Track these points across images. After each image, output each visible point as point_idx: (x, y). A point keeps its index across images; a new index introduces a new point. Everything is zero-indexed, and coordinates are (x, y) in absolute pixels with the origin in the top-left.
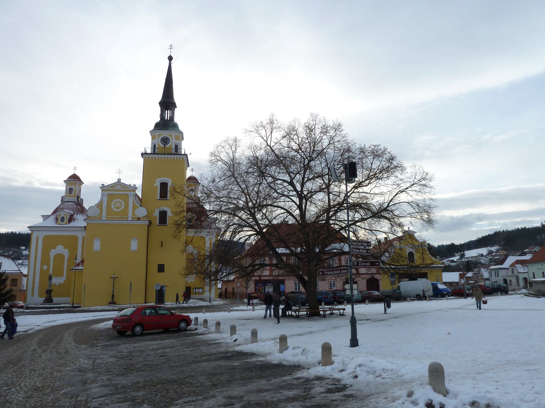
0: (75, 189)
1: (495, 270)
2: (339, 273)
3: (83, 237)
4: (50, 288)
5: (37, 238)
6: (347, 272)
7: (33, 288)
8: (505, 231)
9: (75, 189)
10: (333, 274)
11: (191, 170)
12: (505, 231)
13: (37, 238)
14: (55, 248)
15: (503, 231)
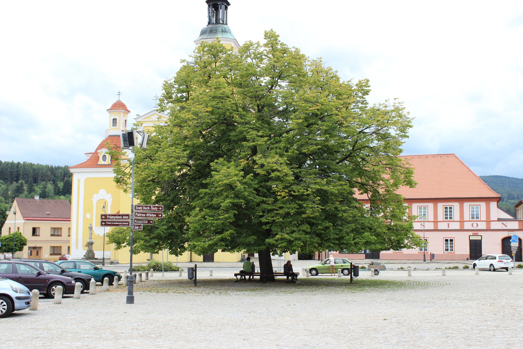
0: (120, 120)
1: (478, 228)
2: (120, 219)
3: (78, 180)
4: (91, 240)
5: (79, 181)
6: (128, 218)
7: (77, 240)
8: (54, 167)
9: (120, 120)
10: (115, 219)
11: (118, 94)
12: (54, 167)
13: (79, 181)
14: (97, 193)
15: (52, 167)
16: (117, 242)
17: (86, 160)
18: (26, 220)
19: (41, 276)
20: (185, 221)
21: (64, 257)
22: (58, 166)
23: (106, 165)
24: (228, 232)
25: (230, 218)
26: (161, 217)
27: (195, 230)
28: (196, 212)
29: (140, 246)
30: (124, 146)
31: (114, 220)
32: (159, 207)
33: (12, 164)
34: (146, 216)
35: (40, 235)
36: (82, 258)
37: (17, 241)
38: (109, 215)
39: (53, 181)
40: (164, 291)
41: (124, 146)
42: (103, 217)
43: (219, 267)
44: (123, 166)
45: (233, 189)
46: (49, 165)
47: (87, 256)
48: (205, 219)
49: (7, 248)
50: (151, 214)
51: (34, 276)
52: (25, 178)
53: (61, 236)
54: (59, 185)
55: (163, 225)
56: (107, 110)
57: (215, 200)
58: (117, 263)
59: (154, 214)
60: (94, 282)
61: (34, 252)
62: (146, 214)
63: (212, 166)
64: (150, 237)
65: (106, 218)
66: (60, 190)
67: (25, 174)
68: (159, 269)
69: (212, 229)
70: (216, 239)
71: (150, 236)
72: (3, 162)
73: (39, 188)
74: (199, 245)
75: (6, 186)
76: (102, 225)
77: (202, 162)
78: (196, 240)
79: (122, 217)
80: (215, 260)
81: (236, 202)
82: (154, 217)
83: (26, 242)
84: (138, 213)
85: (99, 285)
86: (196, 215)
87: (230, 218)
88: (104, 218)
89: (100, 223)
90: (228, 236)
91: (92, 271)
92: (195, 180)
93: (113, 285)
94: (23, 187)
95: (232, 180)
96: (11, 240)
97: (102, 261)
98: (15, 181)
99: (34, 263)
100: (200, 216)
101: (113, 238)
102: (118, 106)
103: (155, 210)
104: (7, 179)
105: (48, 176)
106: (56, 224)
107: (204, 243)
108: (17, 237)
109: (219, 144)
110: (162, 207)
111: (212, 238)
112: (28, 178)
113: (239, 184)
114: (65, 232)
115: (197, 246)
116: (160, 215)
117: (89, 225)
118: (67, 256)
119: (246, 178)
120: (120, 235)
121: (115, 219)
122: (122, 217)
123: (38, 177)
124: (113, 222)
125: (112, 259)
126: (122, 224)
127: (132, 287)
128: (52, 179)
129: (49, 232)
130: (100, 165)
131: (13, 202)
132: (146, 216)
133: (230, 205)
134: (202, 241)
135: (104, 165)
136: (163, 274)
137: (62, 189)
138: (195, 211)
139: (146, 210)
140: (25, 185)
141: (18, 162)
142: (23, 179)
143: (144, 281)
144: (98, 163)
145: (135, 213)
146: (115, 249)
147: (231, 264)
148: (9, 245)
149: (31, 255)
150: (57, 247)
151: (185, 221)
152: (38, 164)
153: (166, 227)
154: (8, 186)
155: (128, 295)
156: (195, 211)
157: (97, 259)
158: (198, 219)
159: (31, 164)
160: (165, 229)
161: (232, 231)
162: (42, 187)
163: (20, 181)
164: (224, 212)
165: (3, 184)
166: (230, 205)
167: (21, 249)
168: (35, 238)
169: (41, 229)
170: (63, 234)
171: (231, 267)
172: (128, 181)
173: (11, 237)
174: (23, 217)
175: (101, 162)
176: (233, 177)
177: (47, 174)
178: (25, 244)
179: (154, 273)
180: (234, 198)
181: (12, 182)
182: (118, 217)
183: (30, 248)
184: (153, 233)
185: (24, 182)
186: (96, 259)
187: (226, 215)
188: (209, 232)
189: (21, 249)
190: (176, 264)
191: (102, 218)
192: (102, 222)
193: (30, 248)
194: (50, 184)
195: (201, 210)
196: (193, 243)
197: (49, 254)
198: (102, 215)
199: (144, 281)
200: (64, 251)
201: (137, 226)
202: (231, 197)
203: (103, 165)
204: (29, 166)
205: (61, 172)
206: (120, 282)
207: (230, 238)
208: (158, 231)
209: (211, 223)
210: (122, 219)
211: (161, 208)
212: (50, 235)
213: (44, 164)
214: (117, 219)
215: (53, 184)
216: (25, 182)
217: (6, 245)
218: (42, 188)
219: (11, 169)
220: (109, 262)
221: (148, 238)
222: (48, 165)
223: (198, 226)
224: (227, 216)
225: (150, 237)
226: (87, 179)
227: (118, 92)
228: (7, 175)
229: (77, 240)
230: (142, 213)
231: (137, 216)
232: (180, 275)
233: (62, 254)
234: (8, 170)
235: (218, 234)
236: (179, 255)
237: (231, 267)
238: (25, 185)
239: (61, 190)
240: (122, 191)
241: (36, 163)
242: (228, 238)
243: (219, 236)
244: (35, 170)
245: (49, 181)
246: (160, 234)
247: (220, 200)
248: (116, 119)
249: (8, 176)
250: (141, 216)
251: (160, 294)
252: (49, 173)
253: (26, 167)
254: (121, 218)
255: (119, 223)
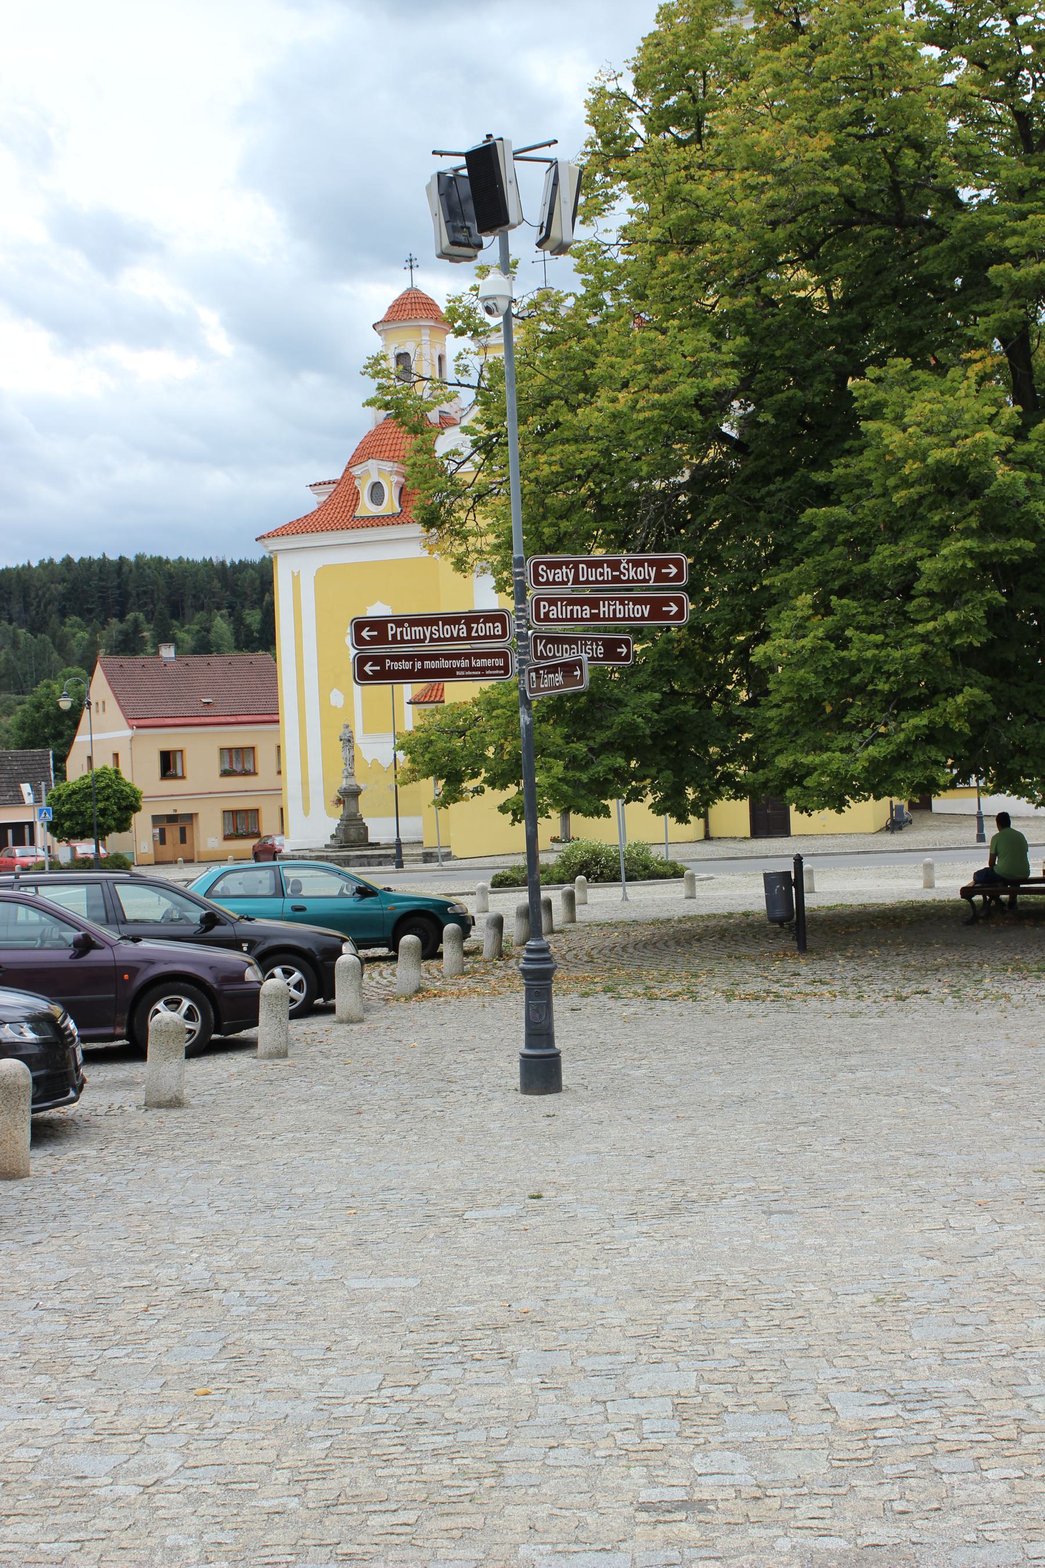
2: (459, 638)
4: (352, 781)
5: (296, 579)
7: (305, 783)
10: (432, 640)
11: (414, 263)
13: (296, 579)
15: (223, 563)
16: (445, 773)
17: (316, 507)
18: (138, 727)
19: (94, 955)
20: (752, 659)
21: (270, 842)
22: (240, 561)
23: (383, 517)
24: (959, 699)
25: (967, 626)
26: (679, 615)
27: (799, 699)
28: (799, 614)
29: (551, 785)
30: (454, 243)
31: (427, 648)
32: (665, 563)
33: (103, 562)
34: (595, 617)
35: (188, 774)
36: (327, 846)
37: (107, 799)
38: (399, 623)
39: (227, 608)
40: (676, 987)
41: (454, 243)
42: (365, 634)
43: (813, 855)
44: (447, 456)
45: (975, 492)
46: (214, 560)
47: (341, 836)
48: (844, 643)
49: (77, 824)
50: (622, 601)
51: (65, 955)
52: (146, 604)
53: (255, 774)
54: (249, 620)
55: (640, 690)
56: (374, 326)
57: (887, 553)
58: (448, 856)
59: (637, 601)
60: (353, 964)
61: (173, 833)
62: (594, 603)
63: (856, 399)
64: (591, 743)
65: (381, 639)
66: (252, 633)
67: (145, 593)
68: (602, 872)
69: (883, 686)
70: (902, 736)
71: (588, 739)
72: (76, 560)
73: (188, 632)
74: (823, 764)
75: (90, 635)
76: (362, 677)
77: (800, 394)
78: (802, 747)
79: (469, 630)
80: (794, 830)
81: (996, 551)
82: (642, 618)
83: (137, 800)
84: (552, 602)
85: (380, 959)
86: (800, 630)
87: (968, 630)
88: (374, 641)
89: (349, 668)
90: (959, 715)
91: (351, 903)
92: (768, 480)
93: (440, 956)
94: (141, 632)
95: (975, 445)
96: (88, 797)
97: (394, 851)
98: (115, 616)
99: (82, 890)
100: (820, 632)
101: (427, 756)
102: (409, 306)
103: (645, 581)
104: (90, 611)
105: (214, 594)
106: (237, 737)
107: (846, 757)
108: (108, 786)
109: (862, 314)
110: (678, 563)
111: (882, 729)
112: (152, 602)
113: (1002, 472)
114: (264, 760)
115: (815, 769)
116: (674, 609)
117: (341, 731)
118: (277, 841)
119: (1031, 435)
120: (458, 743)
121: (432, 640)
122: (469, 630)
123: (182, 601)
124: (423, 658)
125: (430, 842)
126: (471, 669)
127: (549, 1006)
128: (225, 603)
129: (214, 764)
130: (363, 518)
131: (91, 673)
132: (595, 617)
133: (970, 565)
134: (833, 746)
135: (378, 517)
136: (625, 893)
137: (258, 632)
138: (793, 609)
139: (597, 582)
140: (145, 626)
141: (121, 558)
142: (140, 608)
143: (561, 932)
144: (357, 514)
145: (538, 601)
146: (434, 802)
147: (854, 840)
148: (81, 813)
149: (163, 841)
150: (246, 811)
151: (752, 659)
152: (180, 558)
153: (657, 695)
154: (94, 632)
155: (529, 1045)
156: (793, 609)
157: (378, 844)
158: (809, 646)
159: (160, 558)
160: (651, 705)
161: (976, 691)
162: (197, 627)
163: (130, 616)
164: (931, 607)
165: (80, 627)
166: (970, 565)
167: (125, 825)
168: (171, 786)
169: (187, 755)
170: (260, 769)
171: (858, 853)
172: (470, 525)
173: (87, 788)
174: (128, 719)
175: (367, 507)
176: (974, 432)
177: (208, 586)
178: (136, 808)
179: (590, 891)
180: (981, 533)
181: (106, 619)
182: (448, 631)
183: (156, 819)
184: (600, 727)
185: (141, 616)
186: (372, 844)
187: (951, 616)
188: (864, 706)
189: (123, 825)
190: (663, 848)
191: (359, 641)
192: (361, 661)
193: (156, 819)
194: (222, 616)
195: (823, 608)
196: (791, 758)
197: (221, 836)
198: (359, 626)
199: (561, 932)
200: (267, 825)
201: (552, 669)
202: (967, 533)
203: (373, 517)
204: (153, 567)
205: (253, 581)
206: (467, 945)
207: (967, 729)
208: (625, 716)
209: (875, 659)
210: (469, 637)
211: (674, 571)
212: (218, 772)
213: (199, 559)
214: (439, 639)
215: (230, 616)
216: (146, 616)
217: (74, 813)
218: (198, 632)
219: (101, 579)
220: (418, 855)
221: (580, 748)
222: (211, 559)
223: (812, 678)
224: (957, 620)
225: (591, 743)
226: (323, 574)
227: (408, 257)
228: (91, 600)
229: (305, 783)
230: (572, 602)
231: (547, 618)
232: (689, 894)
233: (264, 834)
234: (94, 582)
235: (911, 713)
236: (691, 818)
237: (858, 853)
238: (145, 626)
239: (256, 634)
240: (446, 565)
241: (173, 557)
242: (956, 726)
243: (920, 720)
244: (171, 576)
245: (219, 609)
246: (633, 727)
247: (909, 548)
248: (407, 354)
249: (93, 602)
250: (572, 619)
251: (667, 1006)
252: (216, 584)
253: (144, 570)
254: (464, 633)
255: (456, 663)
